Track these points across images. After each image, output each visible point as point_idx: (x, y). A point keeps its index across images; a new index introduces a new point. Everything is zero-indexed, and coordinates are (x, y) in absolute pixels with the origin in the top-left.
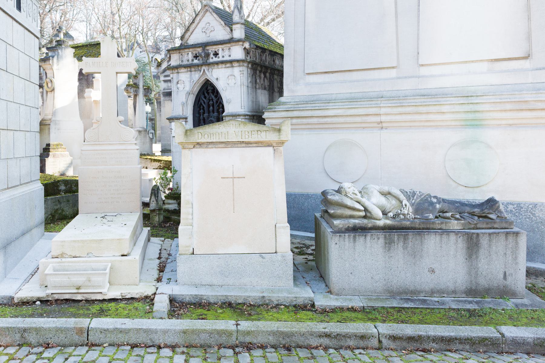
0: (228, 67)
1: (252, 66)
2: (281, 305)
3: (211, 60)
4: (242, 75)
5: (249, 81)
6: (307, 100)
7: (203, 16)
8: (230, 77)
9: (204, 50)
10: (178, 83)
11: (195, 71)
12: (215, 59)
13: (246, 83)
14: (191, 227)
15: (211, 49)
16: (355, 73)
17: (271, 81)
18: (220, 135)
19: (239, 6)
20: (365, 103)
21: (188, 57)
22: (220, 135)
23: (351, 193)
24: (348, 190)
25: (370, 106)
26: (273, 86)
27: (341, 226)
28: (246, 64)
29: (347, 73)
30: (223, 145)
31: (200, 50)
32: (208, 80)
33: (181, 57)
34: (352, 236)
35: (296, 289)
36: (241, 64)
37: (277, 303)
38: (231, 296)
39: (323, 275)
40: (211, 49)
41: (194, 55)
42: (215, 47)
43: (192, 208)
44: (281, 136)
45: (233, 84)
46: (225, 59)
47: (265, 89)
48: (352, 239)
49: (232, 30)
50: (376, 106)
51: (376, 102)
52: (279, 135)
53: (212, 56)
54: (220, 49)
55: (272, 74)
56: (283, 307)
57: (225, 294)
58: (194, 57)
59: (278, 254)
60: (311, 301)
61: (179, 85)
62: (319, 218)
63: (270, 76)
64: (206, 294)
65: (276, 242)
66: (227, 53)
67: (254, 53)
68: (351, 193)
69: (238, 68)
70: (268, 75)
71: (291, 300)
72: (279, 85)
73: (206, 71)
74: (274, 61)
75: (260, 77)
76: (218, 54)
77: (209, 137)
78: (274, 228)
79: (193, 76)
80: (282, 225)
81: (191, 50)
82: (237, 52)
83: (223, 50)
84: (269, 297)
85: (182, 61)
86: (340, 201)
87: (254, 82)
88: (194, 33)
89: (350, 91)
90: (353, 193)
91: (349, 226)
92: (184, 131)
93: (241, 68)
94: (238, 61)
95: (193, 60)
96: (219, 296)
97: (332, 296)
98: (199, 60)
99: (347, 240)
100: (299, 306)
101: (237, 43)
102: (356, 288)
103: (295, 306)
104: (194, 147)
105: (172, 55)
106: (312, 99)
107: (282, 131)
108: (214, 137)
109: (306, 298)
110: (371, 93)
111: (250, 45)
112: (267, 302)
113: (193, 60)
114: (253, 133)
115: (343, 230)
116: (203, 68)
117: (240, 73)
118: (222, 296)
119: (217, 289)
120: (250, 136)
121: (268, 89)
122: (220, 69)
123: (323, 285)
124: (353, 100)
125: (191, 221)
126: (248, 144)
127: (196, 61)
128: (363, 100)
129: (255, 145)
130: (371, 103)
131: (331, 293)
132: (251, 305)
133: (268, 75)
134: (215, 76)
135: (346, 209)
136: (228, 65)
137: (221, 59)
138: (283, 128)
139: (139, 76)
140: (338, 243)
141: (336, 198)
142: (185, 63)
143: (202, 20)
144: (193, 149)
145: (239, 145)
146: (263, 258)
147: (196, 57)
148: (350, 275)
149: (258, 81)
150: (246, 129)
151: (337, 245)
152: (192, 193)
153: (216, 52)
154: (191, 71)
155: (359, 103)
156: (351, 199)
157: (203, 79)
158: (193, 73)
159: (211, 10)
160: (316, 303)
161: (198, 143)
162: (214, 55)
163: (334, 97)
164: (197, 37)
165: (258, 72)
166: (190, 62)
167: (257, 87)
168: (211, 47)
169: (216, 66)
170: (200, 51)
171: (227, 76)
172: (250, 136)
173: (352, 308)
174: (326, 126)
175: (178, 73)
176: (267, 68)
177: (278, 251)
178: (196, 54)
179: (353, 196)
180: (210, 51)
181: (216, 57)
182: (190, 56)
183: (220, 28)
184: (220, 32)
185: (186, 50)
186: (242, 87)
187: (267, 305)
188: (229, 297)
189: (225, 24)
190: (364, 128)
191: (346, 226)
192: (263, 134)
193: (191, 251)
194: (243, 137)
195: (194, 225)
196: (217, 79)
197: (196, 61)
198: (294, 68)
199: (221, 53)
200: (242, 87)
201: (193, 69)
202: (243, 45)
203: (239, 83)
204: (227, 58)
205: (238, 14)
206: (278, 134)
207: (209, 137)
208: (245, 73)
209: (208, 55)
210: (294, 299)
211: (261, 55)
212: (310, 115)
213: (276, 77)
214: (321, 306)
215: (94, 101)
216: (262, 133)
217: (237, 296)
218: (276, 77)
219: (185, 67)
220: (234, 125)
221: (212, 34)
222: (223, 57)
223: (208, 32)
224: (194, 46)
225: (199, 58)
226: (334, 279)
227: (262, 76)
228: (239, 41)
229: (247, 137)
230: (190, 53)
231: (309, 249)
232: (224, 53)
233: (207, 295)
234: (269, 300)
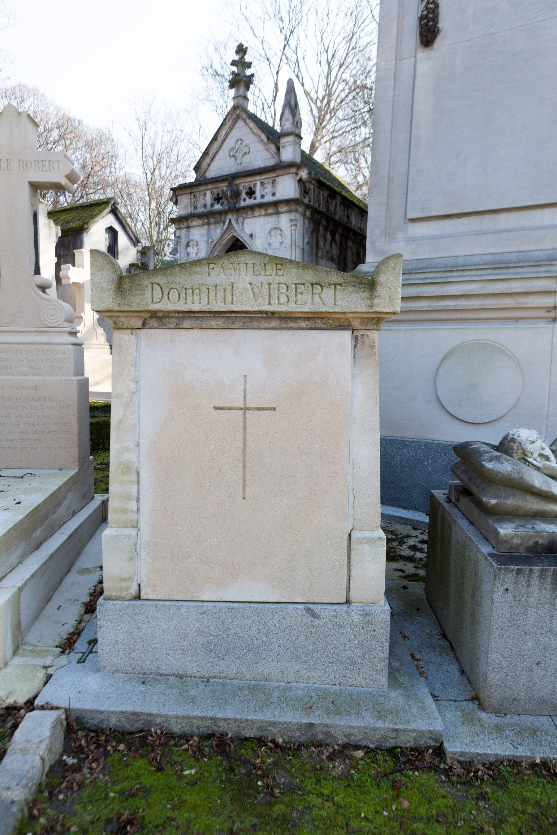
0: (271, 214)
1: (312, 214)
2: (358, 747)
3: (242, 204)
4: (293, 228)
5: (306, 241)
6: (410, 267)
7: (231, 128)
8: (272, 233)
9: (230, 185)
10: (188, 245)
11: (216, 223)
12: (250, 202)
13: (299, 242)
14: (133, 532)
15: (243, 184)
16: (504, 216)
17: (343, 249)
18: (212, 294)
19: (293, 103)
20: (525, 270)
21: (206, 199)
22: (212, 294)
23: (535, 455)
24: (530, 447)
25: (535, 275)
26: (345, 259)
27: (516, 541)
28: (301, 209)
29: (488, 217)
30: (220, 322)
31: (223, 186)
32: (238, 240)
33: (193, 200)
34: (549, 574)
35: (396, 698)
36: (293, 207)
37: (345, 740)
38: (225, 720)
39: (467, 669)
40: (243, 184)
41: (215, 196)
42: (249, 179)
43: (138, 483)
44: (376, 301)
45: (278, 245)
46: (265, 200)
47: (332, 260)
48: (548, 580)
49: (278, 149)
50: (549, 275)
51: (548, 268)
52: (371, 298)
53: (244, 195)
54: (258, 183)
55: (345, 238)
56: (360, 754)
57: (211, 714)
58: (215, 199)
59: (353, 606)
60: (436, 740)
61: (190, 249)
62: (446, 505)
63: (341, 241)
64: (163, 713)
65: (349, 575)
66: (269, 189)
67: (317, 194)
68: (535, 455)
69: (287, 214)
70: (337, 237)
71: (383, 737)
72: (355, 258)
73: (233, 222)
74: (348, 217)
75: (325, 239)
76: (254, 193)
77: (183, 296)
78: (346, 543)
79: (212, 231)
80: (367, 534)
81: (210, 187)
82: (287, 187)
83: (262, 184)
84: (327, 726)
85: (196, 208)
86: (515, 476)
87: (315, 245)
88: (216, 158)
89: (492, 250)
90: (541, 455)
91: (536, 543)
92: (114, 277)
93: (293, 216)
94: (287, 202)
95: (212, 205)
96: (196, 718)
97: (483, 715)
98: (222, 204)
99: (535, 582)
100: (403, 753)
101: (288, 171)
102: (546, 697)
103: (391, 751)
104: (144, 325)
105: (179, 198)
106: (420, 266)
107: (378, 287)
108: (196, 297)
109: (421, 733)
110: (536, 253)
111: (309, 173)
112: (321, 737)
113: (212, 205)
114: (301, 288)
115: (522, 550)
116: (229, 216)
117: (290, 224)
118: (203, 718)
119: (193, 693)
120: (293, 298)
121: (337, 261)
122: (257, 219)
123: (454, 668)
124: (499, 266)
125: (134, 517)
126: (286, 320)
127: (217, 207)
128: (520, 264)
129: (304, 324)
130: (537, 269)
131: (481, 707)
132: (277, 745)
133: (337, 237)
134: (248, 231)
135: (528, 497)
136: (270, 210)
137: (259, 200)
138: (382, 278)
139: (148, 253)
140: (511, 588)
141: (504, 467)
142: (200, 210)
143: (230, 136)
144: (144, 332)
145: (264, 324)
146: (314, 615)
147: (218, 199)
148: (534, 667)
149: (321, 243)
150: (282, 279)
151: (510, 595)
152: (138, 445)
153: (250, 188)
154: (209, 224)
155: (512, 271)
156: (538, 469)
157: (228, 237)
158: (212, 227)
159: (244, 116)
160: (451, 747)
161: (154, 315)
162: (247, 194)
163: (461, 261)
164: (222, 165)
165: (321, 229)
166: (209, 208)
167: (320, 254)
168: (243, 180)
169: (249, 212)
170: (225, 189)
171: (268, 231)
172: (293, 298)
173: (544, 764)
174: (444, 316)
175: (188, 227)
176: (337, 224)
177: (352, 599)
178: (218, 194)
179: (540, 463)
180: (241, 188)
181: (250, 198)
182: (209, 198)
183: (260, 147)
184: (260, 156)
185: (202, 188)
186: (293, 248)
187: (319, 745)
188: (221, 723)
189: (268, 139)
190: (517, 319)
191: (531, 543)
192: (328, 293)
193: (134, 590)
194: (274, 300)
195: (143, 525)
196: (251, 236)
197: (217, 207)
198: (387, 209)
199: (258, 191)
200: (293, 248)
201: (212, 220)
202: (297, 174)
203: (288, 242)
204: (269, 198)
205: (291, 118)
206: (366, 294)
207: (183, 296)
208: (300, 224)
209: (237, 195)
210: (392, 735)
211: (327, 201)
212: (414, 295)
213: (350, 243)
214: (462, 754)
215: (73, 283)
216: (326, 290)
217: (241, 721)
218: (350, 243)
219: (200, 216)
220: (250, 266)
221: (246, 159)
222: (263, 196)
223: (239, 156)
224: (216, 180)
225: (223, 200)
226: (491, 675)
227: (329, 237)
228: (291, 165)
229: (283, 299)
230: (208, 193)
231: (405, 546)
232: (264, 192)
233: (164, 716)
234: (326, 733)
